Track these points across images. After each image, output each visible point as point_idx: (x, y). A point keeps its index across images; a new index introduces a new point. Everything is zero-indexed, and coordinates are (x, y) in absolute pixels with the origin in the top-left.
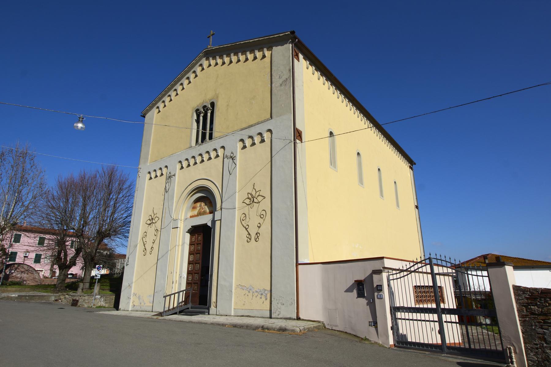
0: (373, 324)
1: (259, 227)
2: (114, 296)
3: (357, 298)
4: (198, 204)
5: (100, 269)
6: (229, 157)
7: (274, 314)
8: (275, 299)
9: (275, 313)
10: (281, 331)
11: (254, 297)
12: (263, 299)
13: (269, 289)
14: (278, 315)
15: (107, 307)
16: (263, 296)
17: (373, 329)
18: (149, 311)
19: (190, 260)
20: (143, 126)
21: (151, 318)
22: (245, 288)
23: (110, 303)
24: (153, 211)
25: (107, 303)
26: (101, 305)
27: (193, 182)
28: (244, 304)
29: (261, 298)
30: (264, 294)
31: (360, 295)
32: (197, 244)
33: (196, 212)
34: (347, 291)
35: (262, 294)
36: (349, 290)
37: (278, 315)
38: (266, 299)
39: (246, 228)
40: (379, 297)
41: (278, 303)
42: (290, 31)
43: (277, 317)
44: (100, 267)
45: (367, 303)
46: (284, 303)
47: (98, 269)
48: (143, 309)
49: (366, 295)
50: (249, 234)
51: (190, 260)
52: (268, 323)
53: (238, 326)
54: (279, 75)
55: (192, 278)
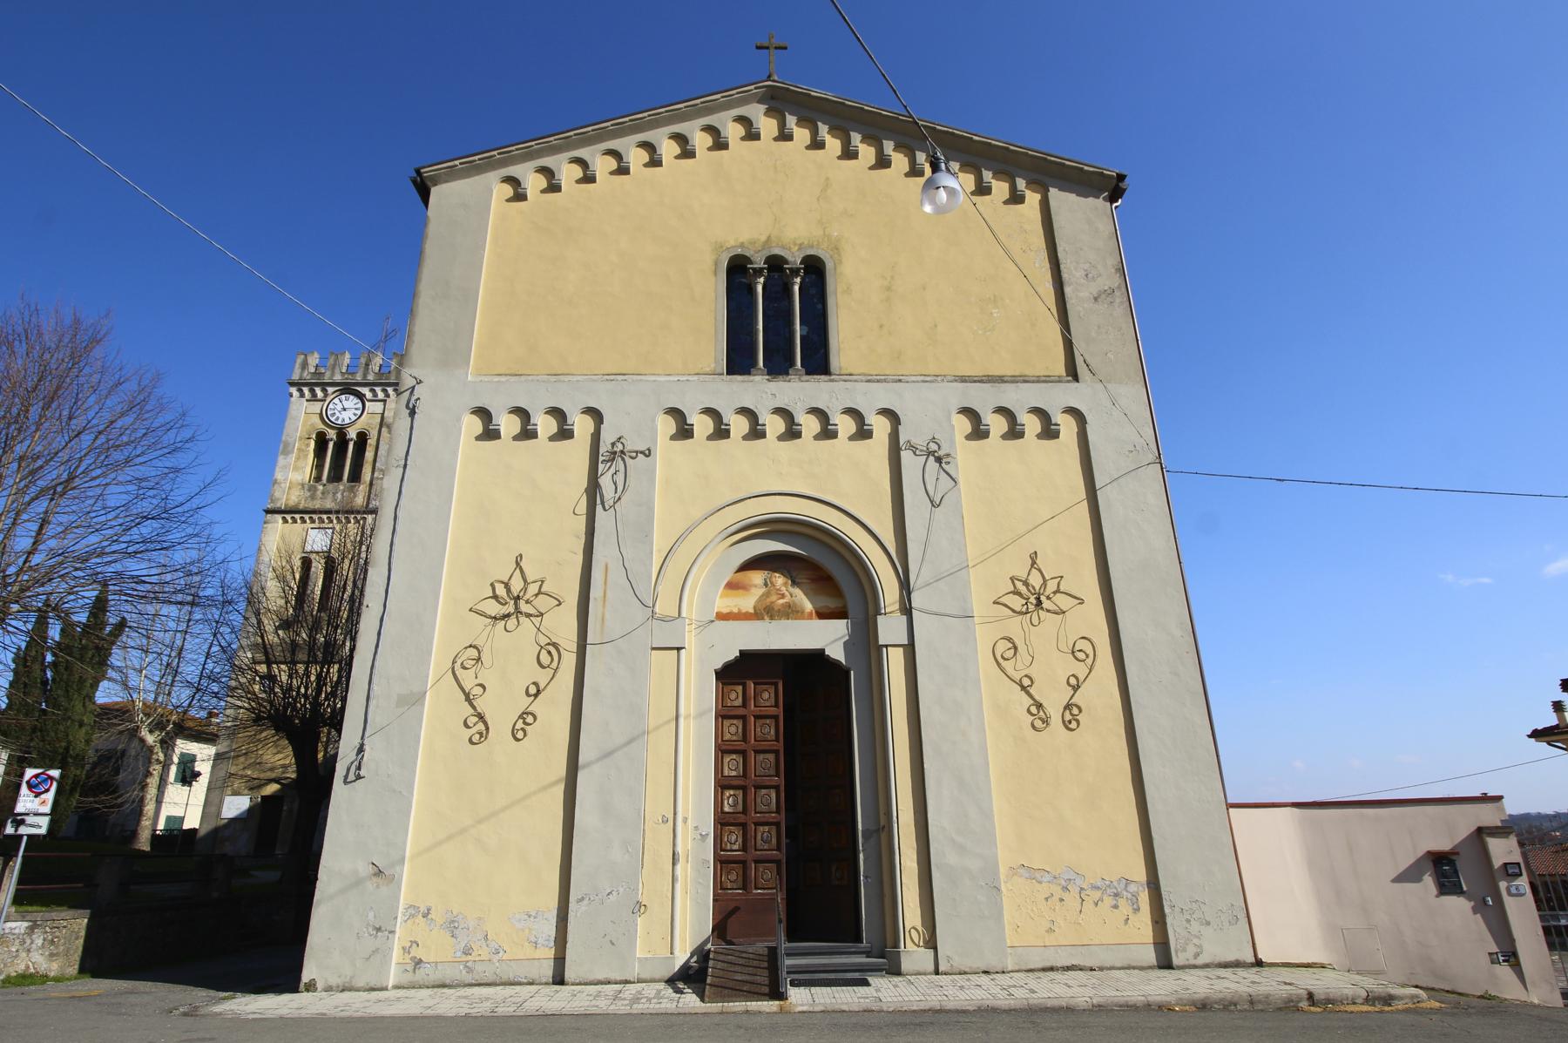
0: (1501, 958)
1: (1076, 688)
2: (86, 920)
3: (1437, 896)
4: (757, 577)
5: (47, 791)
6: (921, 451)
7: (1179, 954)
8: (1177, 909)
9: (1184, 950)
10: (1377, 1002)
11: (1088, 905)
12: (1125, 908)
13: (1141, 875)
14: (1196, 955)
15: (52, 974)
16: (1122, 902)
17: (1505, 971)
19: (726, 773)
20: (424, 222)
21: (722, 1013)
22: (1047, 878)
23: (67, 953)
25: (57, 955)
26: (28, 967)
27: (750, 498)
28: (1051, 930)
29: (1116, 907)
30: (1125, 893)
32: (756, 717)
33: (747, 603)
34: (1400, 879)
35: (1116, 895)
36: (1409, 875)
37: (1196, 955)
40: (1513, 891)
41: (1188, 921)
42: (1117, 171)
43: (1193, 962)
44: (45, 780)
45: (1473, 908)
46: (1208, 919)
47: (35, 786)
49: (1465, 888)
50: (1039, 706)
51: (726, 773)
52: (1161, 987)
53: (1216, 1003)
54: (1086, 270)
55: (740, 840)
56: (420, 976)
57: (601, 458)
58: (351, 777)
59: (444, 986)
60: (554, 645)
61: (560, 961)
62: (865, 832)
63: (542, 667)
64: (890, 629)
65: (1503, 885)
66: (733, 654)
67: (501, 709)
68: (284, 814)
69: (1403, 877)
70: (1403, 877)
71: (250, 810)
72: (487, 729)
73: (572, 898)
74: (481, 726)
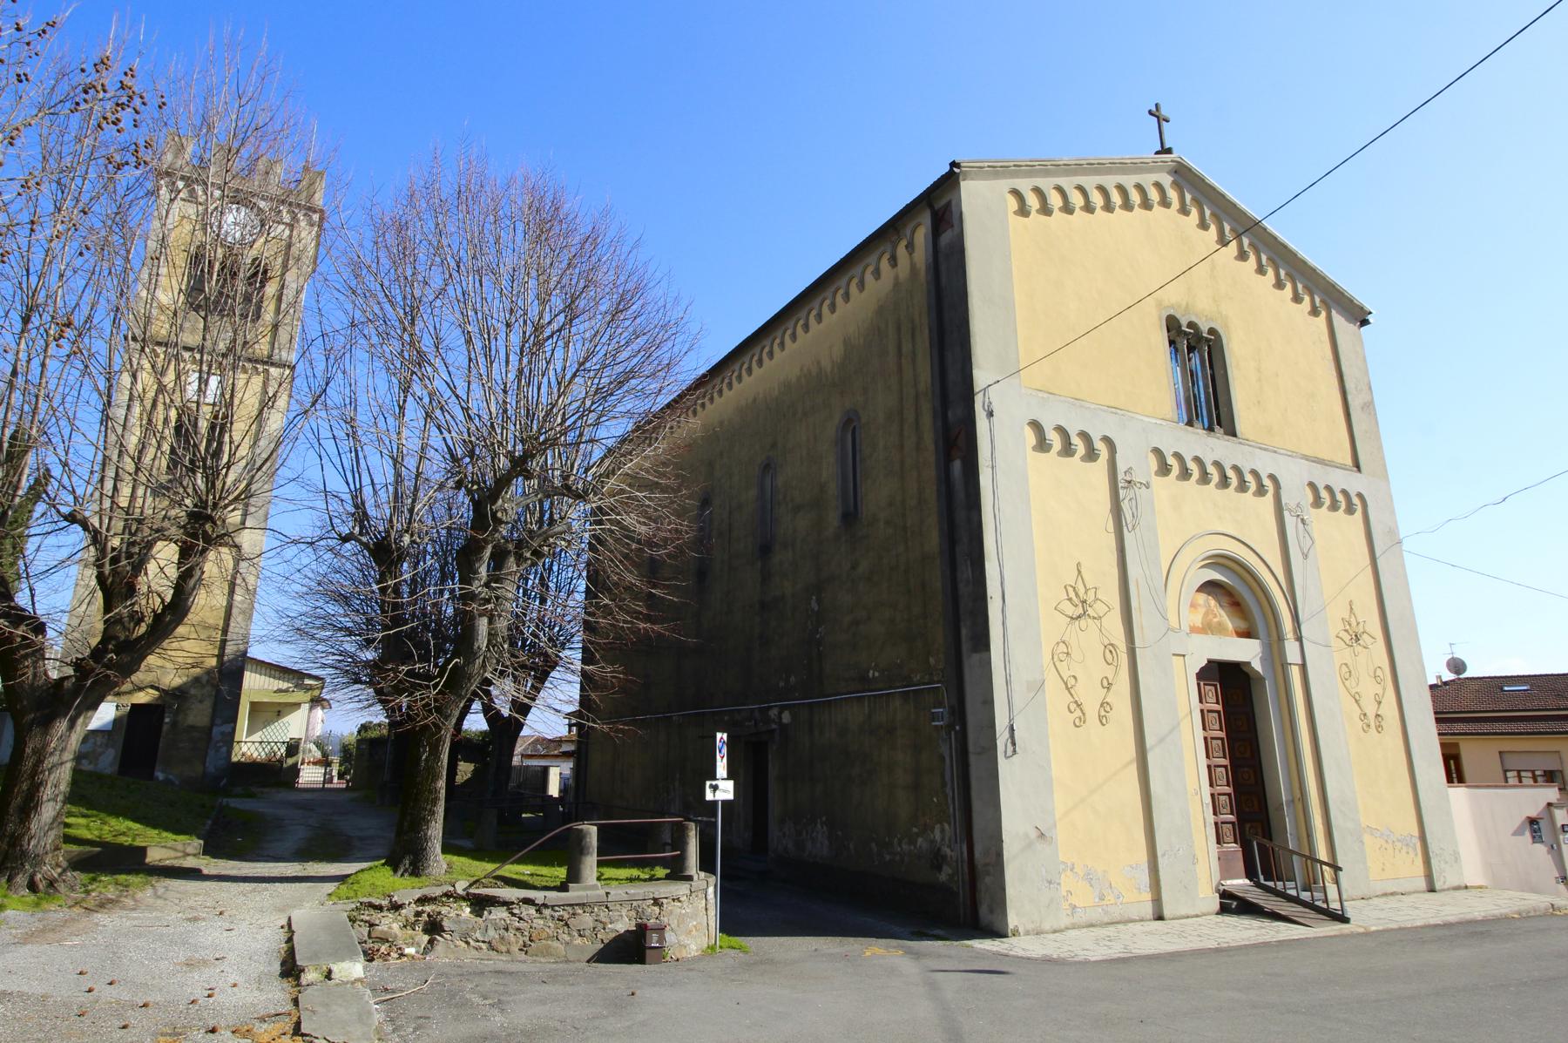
12: (1412, 855)
13: (1416, 832)
18: (1142, 920)
24: (1079, 572)
31: (1536, 836)
36: (1518, 832)
38: (1416, 855)
39: (1066, 684)
48: (1116, 913)
56: (1076, 919)
57: (1120, 485)
58: (1009, 752)
59: (1092, 925)
60: (1112, 645)
61: (1157, 901)
62: (1287, 801)
63: (1108, 664)
64: (1292, 651)
65: (1561, 837)
66: (1204, 663)
67: (1091, 697)
68: (165, 728)
69: (1516, 833)
70: (1516, 833)
71: (116, 721)
72: (1084, 714)
73: (1159, 854)
74: (1078, 713)
